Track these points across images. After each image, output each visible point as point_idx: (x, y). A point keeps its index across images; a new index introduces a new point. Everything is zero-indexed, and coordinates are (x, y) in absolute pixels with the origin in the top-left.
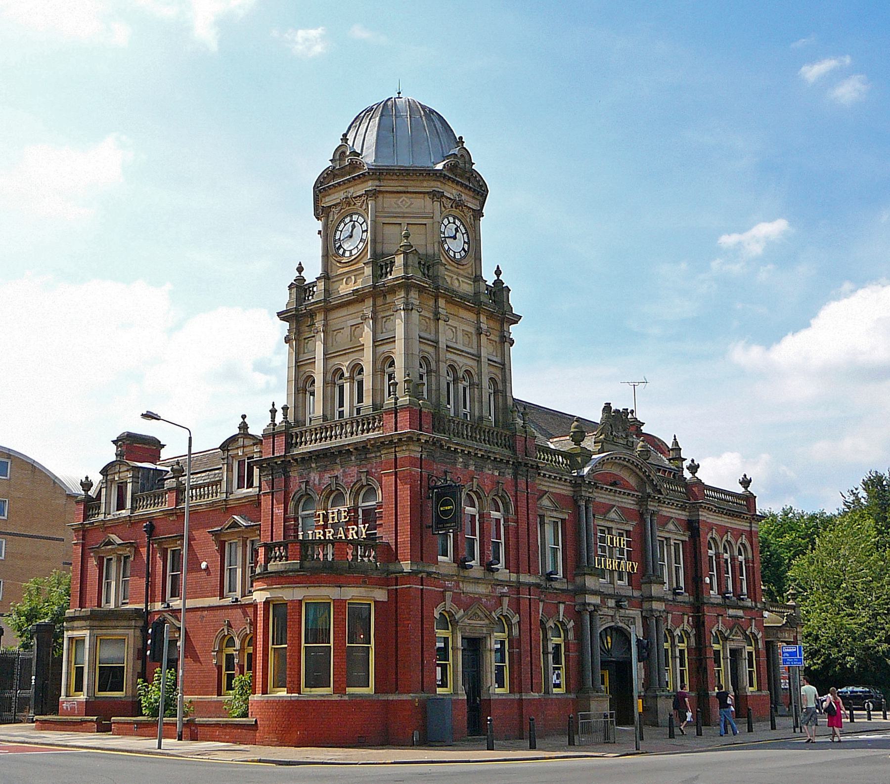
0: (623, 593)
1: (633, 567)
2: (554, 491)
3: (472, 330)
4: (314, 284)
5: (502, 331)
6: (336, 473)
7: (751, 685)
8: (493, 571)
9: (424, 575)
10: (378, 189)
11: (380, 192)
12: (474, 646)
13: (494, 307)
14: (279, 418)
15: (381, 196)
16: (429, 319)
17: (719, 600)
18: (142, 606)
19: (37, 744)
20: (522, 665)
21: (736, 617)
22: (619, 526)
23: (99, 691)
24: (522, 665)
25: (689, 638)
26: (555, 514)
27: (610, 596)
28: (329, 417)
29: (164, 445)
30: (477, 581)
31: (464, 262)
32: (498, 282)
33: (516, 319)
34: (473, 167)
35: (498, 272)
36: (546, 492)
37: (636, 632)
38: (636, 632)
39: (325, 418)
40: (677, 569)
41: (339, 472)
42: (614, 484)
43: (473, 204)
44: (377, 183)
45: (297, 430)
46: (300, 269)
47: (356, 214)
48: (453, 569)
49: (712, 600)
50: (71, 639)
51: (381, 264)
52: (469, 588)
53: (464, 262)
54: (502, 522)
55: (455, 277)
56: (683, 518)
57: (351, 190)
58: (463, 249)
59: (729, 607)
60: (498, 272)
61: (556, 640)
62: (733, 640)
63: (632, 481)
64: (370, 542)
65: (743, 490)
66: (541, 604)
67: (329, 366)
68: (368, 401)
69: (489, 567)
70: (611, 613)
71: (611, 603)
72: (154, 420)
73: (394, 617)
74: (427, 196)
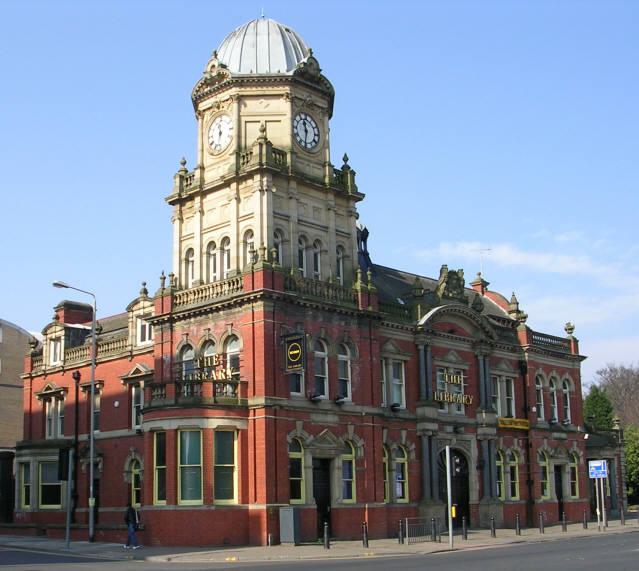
0: (460, 421)
1: (468, 400)
2: (398, 337)
6: (209, 326)
7: (574, 493)
8: (340, 404)
9: (278, 408)
10: (241, 93)
11: (242, 96)
12: (559, 469)
13: (343, 188)
14: (167, 284)
17: (547, 426)
18: (72, 437)
19: (17, 547)
20: (373, 476)
21: (561, 439)
22: (457, 366)
23: (43, 503)
24: (373, 476)
25: (578, 458)
26: (398, 357)
27: (449, 423)
28: (205, 281)
29: (584, 358)
30: (326, 412)
31: (315, 151)
32: (346, 167)
33: (360, 197)
34: (322, 73)
35: (346, 159)
36: (390, 338)
37: (473, 454)
38: (473, 454)
40: (509, 401)
41: (210, 325)
42: (452, 332)
44: (238, 89)
45: (180, 293)
48: (305, 404)
49: (538, 425)
50: (21, 464)
51: (241, 153)
53: (315, 151)
54: (326, 360)
55: (306, 163)
56: (513, 358)
57: (220, 96)
58: (314, 140)
59: (554, 431)
60: (346, 159)
61: (400, 460)
62: (558, 458)
63: (468, 329)
64: (234, 382)
66: (385, 431)
67: (204, 241)
69: (336, 401)
71: (450, 429)
72: (64, 288)
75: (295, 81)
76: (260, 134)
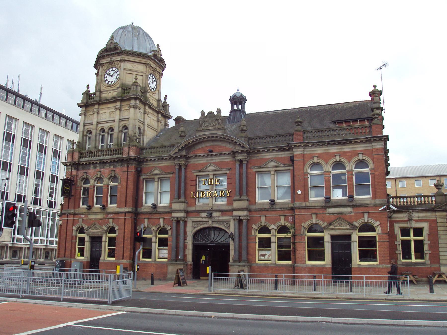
3: (156, 119)
4: (94, 94)
5: (165, 121)
15: (126, 62)
30: (96, 213)
32: (165, 102)
35: (165, 99)
39: (95, 147)
43: (160, 70)
46: (88, 87)
47: (115, 68)
52: (92, 217)
56: (285, 156)
60: (165, 99)
65: (437, 190)
68: (114, 142)
70: (206, 220)
71: (204, 215)
73: (126, 233)
74: (144, 65)
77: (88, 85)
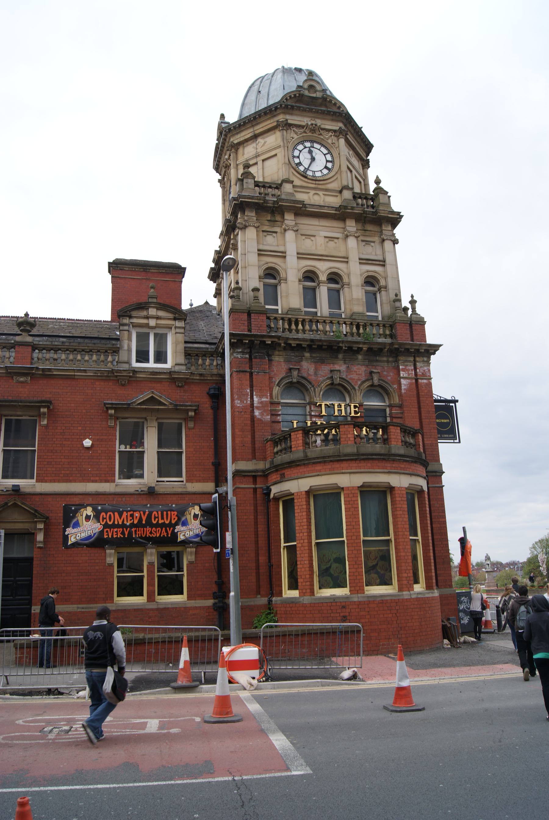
16: (338, 238)
75: (287, 106)
76: (375, 186)
77: (377, 177)
